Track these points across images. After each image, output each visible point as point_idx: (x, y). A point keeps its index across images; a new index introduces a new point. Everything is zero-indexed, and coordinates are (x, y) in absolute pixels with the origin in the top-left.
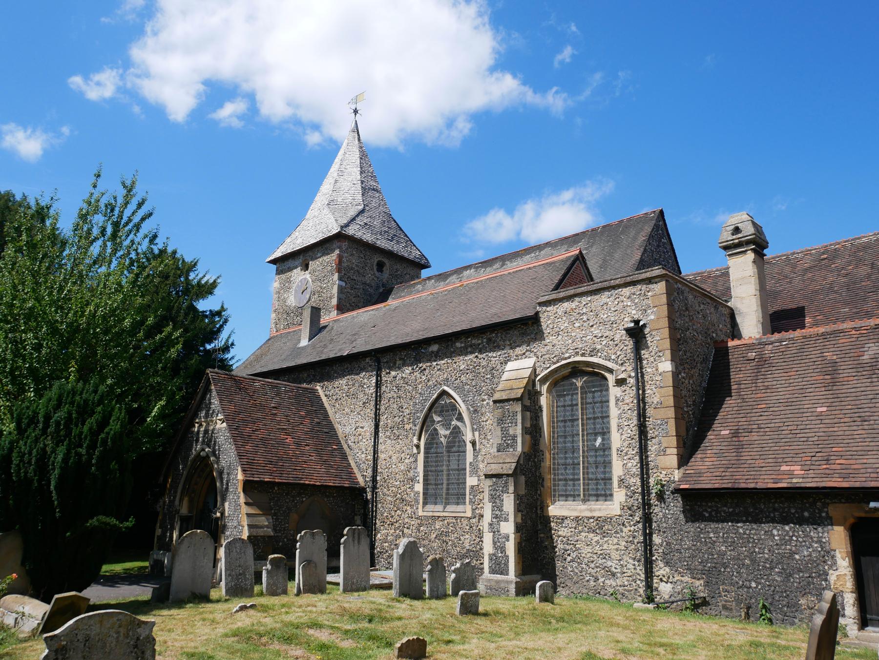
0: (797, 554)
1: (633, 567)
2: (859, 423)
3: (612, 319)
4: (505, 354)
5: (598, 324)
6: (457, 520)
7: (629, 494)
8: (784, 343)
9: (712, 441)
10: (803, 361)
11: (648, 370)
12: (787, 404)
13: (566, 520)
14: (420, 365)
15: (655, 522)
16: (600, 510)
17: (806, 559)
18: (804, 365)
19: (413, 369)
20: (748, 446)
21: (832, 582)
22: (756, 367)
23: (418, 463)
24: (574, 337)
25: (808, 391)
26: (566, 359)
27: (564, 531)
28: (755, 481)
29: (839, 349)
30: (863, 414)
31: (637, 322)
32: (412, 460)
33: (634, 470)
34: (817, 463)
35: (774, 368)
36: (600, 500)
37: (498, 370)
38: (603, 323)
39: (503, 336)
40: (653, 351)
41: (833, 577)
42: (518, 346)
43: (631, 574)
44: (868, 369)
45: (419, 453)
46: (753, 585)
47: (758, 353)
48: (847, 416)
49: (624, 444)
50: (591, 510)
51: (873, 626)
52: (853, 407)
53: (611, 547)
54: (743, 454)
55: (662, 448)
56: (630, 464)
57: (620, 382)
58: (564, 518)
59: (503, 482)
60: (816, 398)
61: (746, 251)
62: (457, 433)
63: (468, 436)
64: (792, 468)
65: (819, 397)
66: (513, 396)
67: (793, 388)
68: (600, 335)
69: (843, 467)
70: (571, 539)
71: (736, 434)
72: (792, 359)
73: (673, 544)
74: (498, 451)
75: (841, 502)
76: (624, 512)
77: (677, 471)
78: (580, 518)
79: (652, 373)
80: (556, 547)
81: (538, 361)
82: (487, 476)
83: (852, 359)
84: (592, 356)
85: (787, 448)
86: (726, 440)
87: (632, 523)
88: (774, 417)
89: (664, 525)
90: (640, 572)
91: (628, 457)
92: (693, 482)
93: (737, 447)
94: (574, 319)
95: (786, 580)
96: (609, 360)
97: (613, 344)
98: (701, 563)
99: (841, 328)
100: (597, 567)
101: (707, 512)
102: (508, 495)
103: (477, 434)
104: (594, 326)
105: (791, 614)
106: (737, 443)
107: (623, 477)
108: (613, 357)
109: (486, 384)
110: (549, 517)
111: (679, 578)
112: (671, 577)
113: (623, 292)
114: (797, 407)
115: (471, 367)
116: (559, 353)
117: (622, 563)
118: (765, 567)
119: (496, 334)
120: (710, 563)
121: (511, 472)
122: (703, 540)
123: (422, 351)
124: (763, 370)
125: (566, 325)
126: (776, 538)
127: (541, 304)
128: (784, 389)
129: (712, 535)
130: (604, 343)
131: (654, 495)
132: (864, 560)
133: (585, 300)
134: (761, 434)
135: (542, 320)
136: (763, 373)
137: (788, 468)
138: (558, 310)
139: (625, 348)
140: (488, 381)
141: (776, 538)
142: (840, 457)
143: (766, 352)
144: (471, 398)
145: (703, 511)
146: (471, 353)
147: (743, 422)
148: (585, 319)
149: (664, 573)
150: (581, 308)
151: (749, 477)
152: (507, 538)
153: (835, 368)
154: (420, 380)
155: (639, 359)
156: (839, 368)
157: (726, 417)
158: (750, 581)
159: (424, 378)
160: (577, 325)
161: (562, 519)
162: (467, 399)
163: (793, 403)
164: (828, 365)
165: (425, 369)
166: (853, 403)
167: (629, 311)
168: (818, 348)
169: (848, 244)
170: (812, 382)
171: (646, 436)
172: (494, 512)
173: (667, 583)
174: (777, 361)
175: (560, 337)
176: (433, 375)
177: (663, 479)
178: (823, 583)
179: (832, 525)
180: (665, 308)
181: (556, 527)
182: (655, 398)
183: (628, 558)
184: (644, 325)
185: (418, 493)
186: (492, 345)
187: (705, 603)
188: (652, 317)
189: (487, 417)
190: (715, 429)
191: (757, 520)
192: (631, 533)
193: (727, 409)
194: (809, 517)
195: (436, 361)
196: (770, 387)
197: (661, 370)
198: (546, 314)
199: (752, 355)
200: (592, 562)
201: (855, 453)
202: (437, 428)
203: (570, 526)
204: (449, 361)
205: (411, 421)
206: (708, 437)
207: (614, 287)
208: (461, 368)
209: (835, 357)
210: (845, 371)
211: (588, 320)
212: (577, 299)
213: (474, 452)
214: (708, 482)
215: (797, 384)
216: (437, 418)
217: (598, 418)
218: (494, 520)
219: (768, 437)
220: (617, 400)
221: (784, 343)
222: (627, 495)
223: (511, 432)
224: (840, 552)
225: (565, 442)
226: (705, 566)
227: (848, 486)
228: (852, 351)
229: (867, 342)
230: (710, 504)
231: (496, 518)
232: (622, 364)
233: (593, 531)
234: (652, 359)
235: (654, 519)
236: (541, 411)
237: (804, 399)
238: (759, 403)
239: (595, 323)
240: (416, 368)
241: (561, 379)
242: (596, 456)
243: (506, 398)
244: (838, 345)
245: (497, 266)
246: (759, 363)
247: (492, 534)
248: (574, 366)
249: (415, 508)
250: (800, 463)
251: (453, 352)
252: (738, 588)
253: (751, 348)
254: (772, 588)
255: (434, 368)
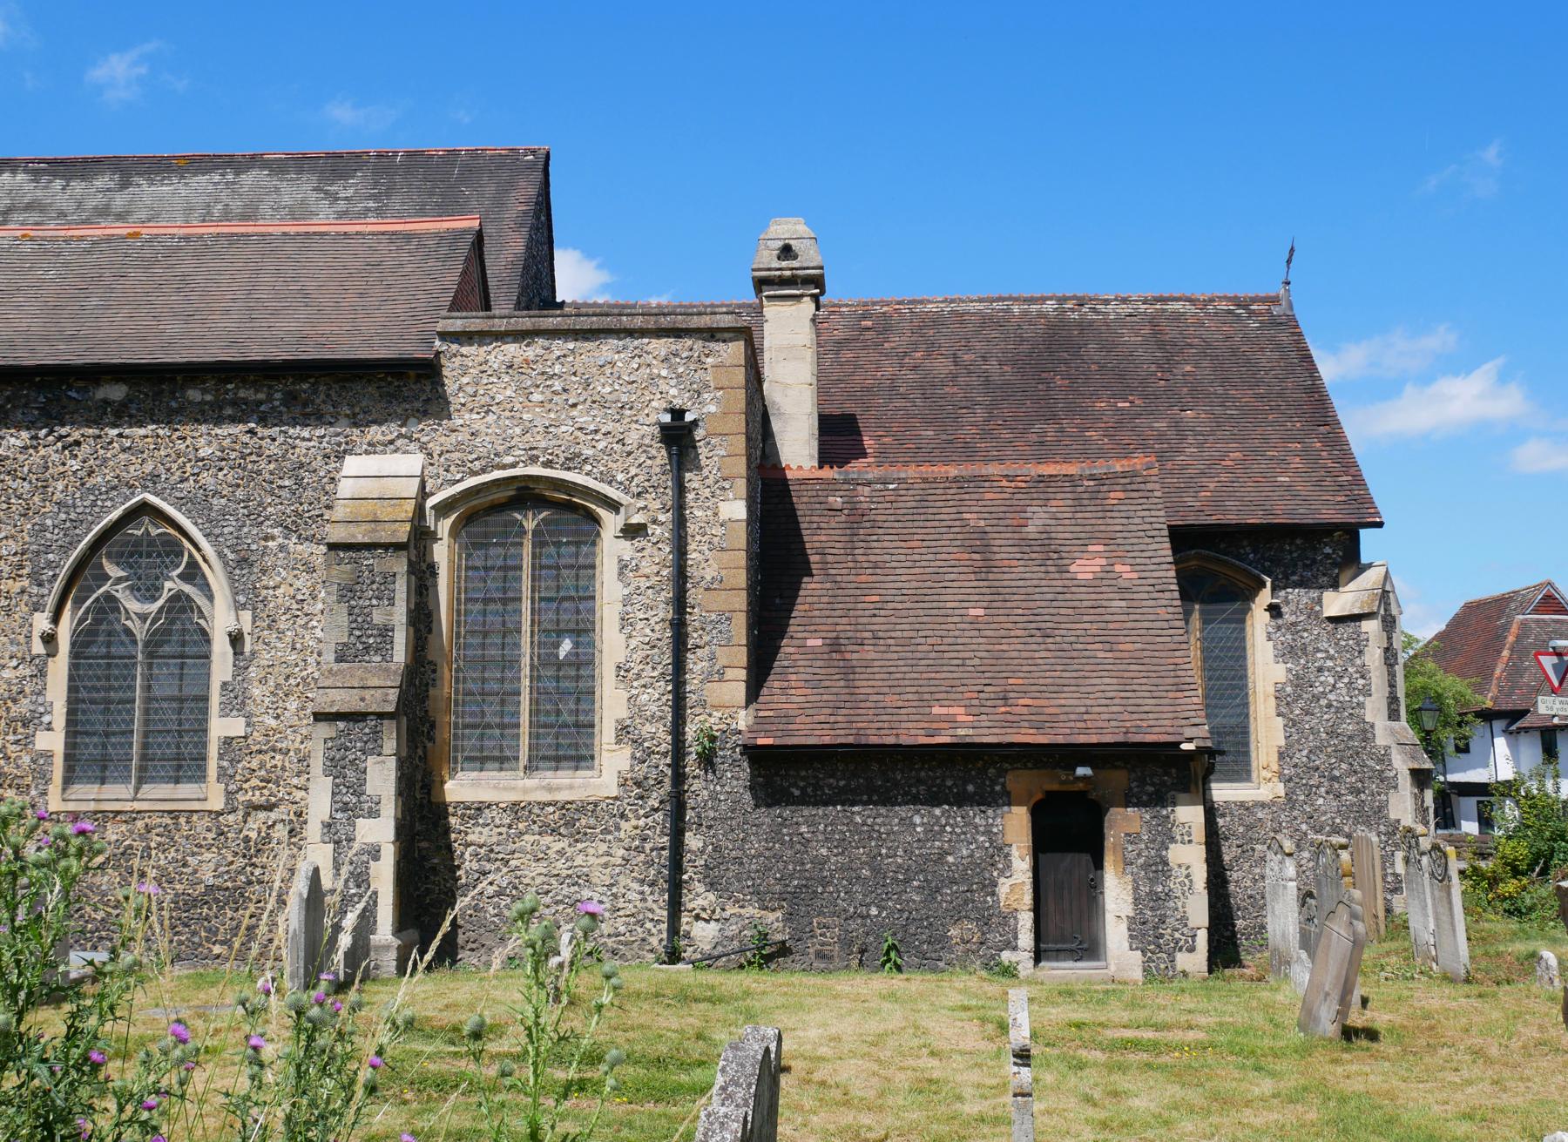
0: (950, 854)
1: (640, 897)
2: (1040, 640)
3: (624, 398)
4: (338, 435)
5: (588, 402)
6: (177, 818)
7: (638, 755)
8: (891, 487)
9: (793, 657)
10: (928, 524)
11: (697, 514)
12: (916, 598)
13: (487, 811)
14: (64, 431)
15: (693, 809)
16: (571, 787)
17: (964, 861)
18: (932, 531)
19: (35, 437)
20: (863, 670)
21: (1002, 897)
22: (849, 525)
23: (49, 678)
24: (527, 424)
25: (948, 577)
26: (504, 467)
27: (481, 833)
28: (894, 732)
29: (986, 509)
30: (1043, 625)
31: (678, 414)
32: (25, 671)
33: (654, 708)
34: (989, 703)
35: (880, 531)
36: (563, 769)
37: (315, 471)
38: (603, 404)
39: (332, 393)
40: (711, 476)
41: (1003, 888)
42: (375, 422)
43: (634, 910)
44: (1038, 549)
45: (52, 654)
46: (874, 911)
47: (846, 499)
48: (1019, 625)
49: (634, 656)
50: (550, 789)
51: (1048, 959)
52: (1026, 612)
53: (592, 860)
54: (858, 683)
55: (717, 668)
56: (646, 696)
57: (632, 532)
58: (481, 808)
59: (367, 730)
60: (963, 591)
61: (802, 296)
62: (183, 610)
63: (221, 618)
64: (952, 711)
65: (968, 591)
66: (384, 536)
67: (922, 570)
68: (592, 427)
69: (1033, 710)
70: (496, 849)
71: (835, 646)
72: (910, 517)
73: (727, 848)
74: (339, 659)
75: (1026, 768)
76: (626, 791)
77: (743, 713)
78: (522, 805)
79: (705, 519)
80: (459, 867)
81: (432, 464)
82: (319, 717)
83: (1010, 529)
84: (569, 469)
85: (933, 675)
86: (819, 656)
87: (641, 812)
88: (899, 621)
89: (712, 814)
90: (654, 906)
91: (642, 682)
92: (779, 734)
93: (843, 670)
94: (529, 383)
95: (929, 898)
96: (610, 483)
97: (623, 451)
98: (780, 880)
99: (984, 472)
100: (557, 903)
101: (798, 787)
102: (380, 758)
103: (247, 616)
104: (580, 407)
105: (933, 955)
106: (841, 664)
107: (628, 722)
108: (620, 477)
109: (277, 501)
110: (445, 805)
111: (736, 910)
112: (718, 910)
113: (651, 346)
114: (935, 605)
115: (233, 455)
116: (489, 453)
117: (614, 890)
118: (897, 880)
119: (313, 385)
120: (799, 879)
121: (391, 708)
122: (787, 838)
123: (73, 394)
124: (862, 531)
125: (509, 393)
126: (918, 829)
127: (445, 336)
128: (907, 571)
129: (804, 829)
130: (601, 445)
131: (694, 756)
132: (1041, 855)
133: (559, 346)
134: (883, 648)
135: (445, 372)
136: (862, 537)
137: (944, 711)
138: (491, 358)
139: (649, 462)
140: (285, 493)
141: (918, 829)
142: (1022, 695)
143: (862, 499)
144: (231, 529)
145: (789, 786)
146: (234, 420)
147: (843, 626)
148: (558, 386)
149: (705, 903)
150: (549, 363)
151: (880, 725)
152: (375, 853)
153: (985, 542)
154: (61, 469)
155: (681, 489)
156: (992, 542)
157: (810, 614)
158: (868, 905)
159: (75, 465)
160: (536, 397)
161: (479, 809)
162: (217, 531)
163: (927, 598)
164: (973, 536)
165: (77, 443)
166: (1024, 605)
167: (663, 387)
168: (951, 503)
169: (904, 309)
170: (953, 563)
171: (685, 644)
172: (338, 798)
173: (707, 921)
174: (884, 518)
175: (491, 418)
176: (105, 460)
177: (715, 728)
178: (989, 898)
179: (1009, 804)
180: (741, 394)
181: (461, 824)
182: (708, 570)
183: (629, 881)
184: (695, 423)
185: (48, 755)
186: (297, 410)
187: (783, 950)
188: (712, 408)
189: (278, 579)
190: (795, 635)
191: (887, 800)
192: (638, 831)
193: (809, 599)
194: (975, 793)
195: (117, 426)
196: (881, 565)
197: (723, 516)
198: (458, 360)
199: (836, 501)
200: (547, 893)
201: (1044, 688)
202: (118, 595)
203: (498, 822)
204: (161, 432)
205: (25, 572)
206: (782, 650)
207: (631, 333)
208: (202, 453)
209: (982, 523)
210: (1004, 552)
211: (565, 390)
212: (541, 341)
213: (235, 660)
214: (809, 732)
215: (927, 564)
216: (113, 571)
217: (493, 600)
218: (339, 815)
219: (895, 656)
220: (623, 567)
221: (891, 487)
222: (633, 757)
223: (378, 617)
224: (1018, 848)
225: (483, 647)
226: (787, 885)
227: (1046, 742)
228: (1008, 515)
229: (1028, 502)
230: (803, 773)
231: (345, 808)
232: (639, 494)
233: (553, 831)
234: (707, 492)
235: (691, 803)
236: (434, 574)
237: (943, 591)
238: (867, 592)
239: (582, 399)
240: (46, 436)
241: (679, 529)
242: (558, 679)
243: (366, 540)
244: (984, 503)
245: (102, 181)
246: (852, 519)
247: (332, 845)
248: (523, 484)
249: (33, 792)
250: (963, 703)
251: (180, 411)
252: (846, 919)
253: (831, 487)
254: (906, 915)
255: (111, 443)
